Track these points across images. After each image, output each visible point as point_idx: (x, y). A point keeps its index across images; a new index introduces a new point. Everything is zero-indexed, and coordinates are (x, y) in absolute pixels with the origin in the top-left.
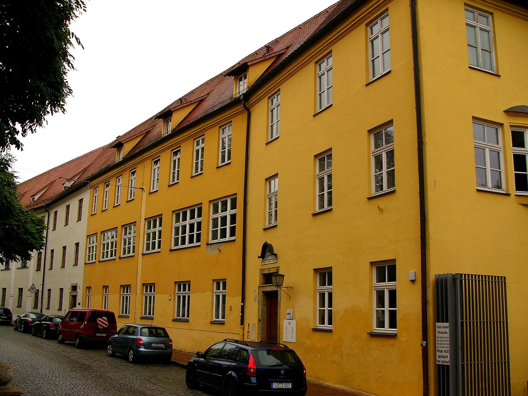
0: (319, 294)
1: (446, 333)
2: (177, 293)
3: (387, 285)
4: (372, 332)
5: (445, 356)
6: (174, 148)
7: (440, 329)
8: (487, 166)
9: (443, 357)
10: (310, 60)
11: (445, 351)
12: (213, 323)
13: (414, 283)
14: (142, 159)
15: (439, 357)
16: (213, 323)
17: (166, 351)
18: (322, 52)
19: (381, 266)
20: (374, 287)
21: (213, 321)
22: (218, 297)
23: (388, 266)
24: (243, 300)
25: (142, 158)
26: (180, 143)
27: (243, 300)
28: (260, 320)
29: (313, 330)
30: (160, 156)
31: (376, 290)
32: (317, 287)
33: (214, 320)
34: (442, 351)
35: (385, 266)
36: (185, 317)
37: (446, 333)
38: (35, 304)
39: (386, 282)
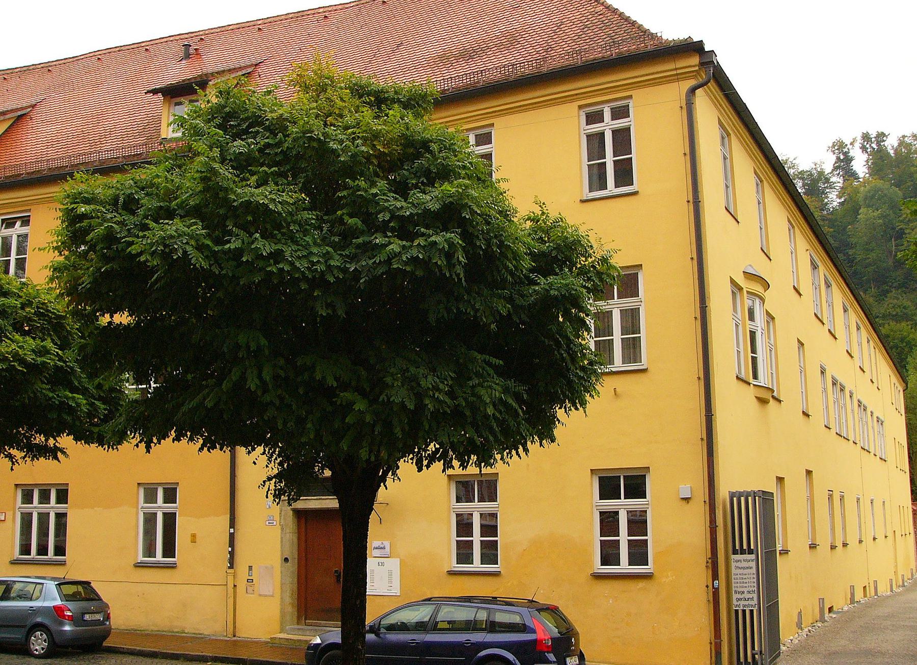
0: (455, 515)
1: (751, 568)
2: (142, 508)
3: (476, 509)
4: (451, 571)
5: (748, 599)
6: (20, 209)
7: (739, 563)
8: (758, 354)
9: (746, 599)
10: (625, 87)
11: (749, 592)
12: (139, 566)
13: (688, 503)
14: (675, 72)
15: (738, 600)
16: (139, 566)
17: (102, 627)
18: (625, 89)
19: (611, 475)
20: (596, 506)
21: (139, 562)
22: (150, 519)
23: (624, 477)
24: (232, 524)
25: (676, 69)
26: (32, 204)
27: (232, 524)
28: (286, 560)
29: (449, 573)
30: (493, 125)
31: (480, 513)
32: (451, 505)
33: (141, 561)
34: (743, 592)
35: (620, 476)
36: (47, 555)
37: (751, 568)
38: (234, 513)
39: (621, 499)
